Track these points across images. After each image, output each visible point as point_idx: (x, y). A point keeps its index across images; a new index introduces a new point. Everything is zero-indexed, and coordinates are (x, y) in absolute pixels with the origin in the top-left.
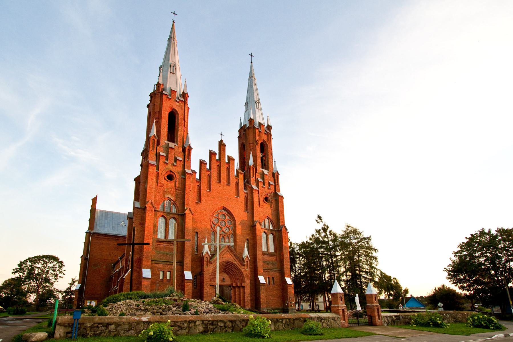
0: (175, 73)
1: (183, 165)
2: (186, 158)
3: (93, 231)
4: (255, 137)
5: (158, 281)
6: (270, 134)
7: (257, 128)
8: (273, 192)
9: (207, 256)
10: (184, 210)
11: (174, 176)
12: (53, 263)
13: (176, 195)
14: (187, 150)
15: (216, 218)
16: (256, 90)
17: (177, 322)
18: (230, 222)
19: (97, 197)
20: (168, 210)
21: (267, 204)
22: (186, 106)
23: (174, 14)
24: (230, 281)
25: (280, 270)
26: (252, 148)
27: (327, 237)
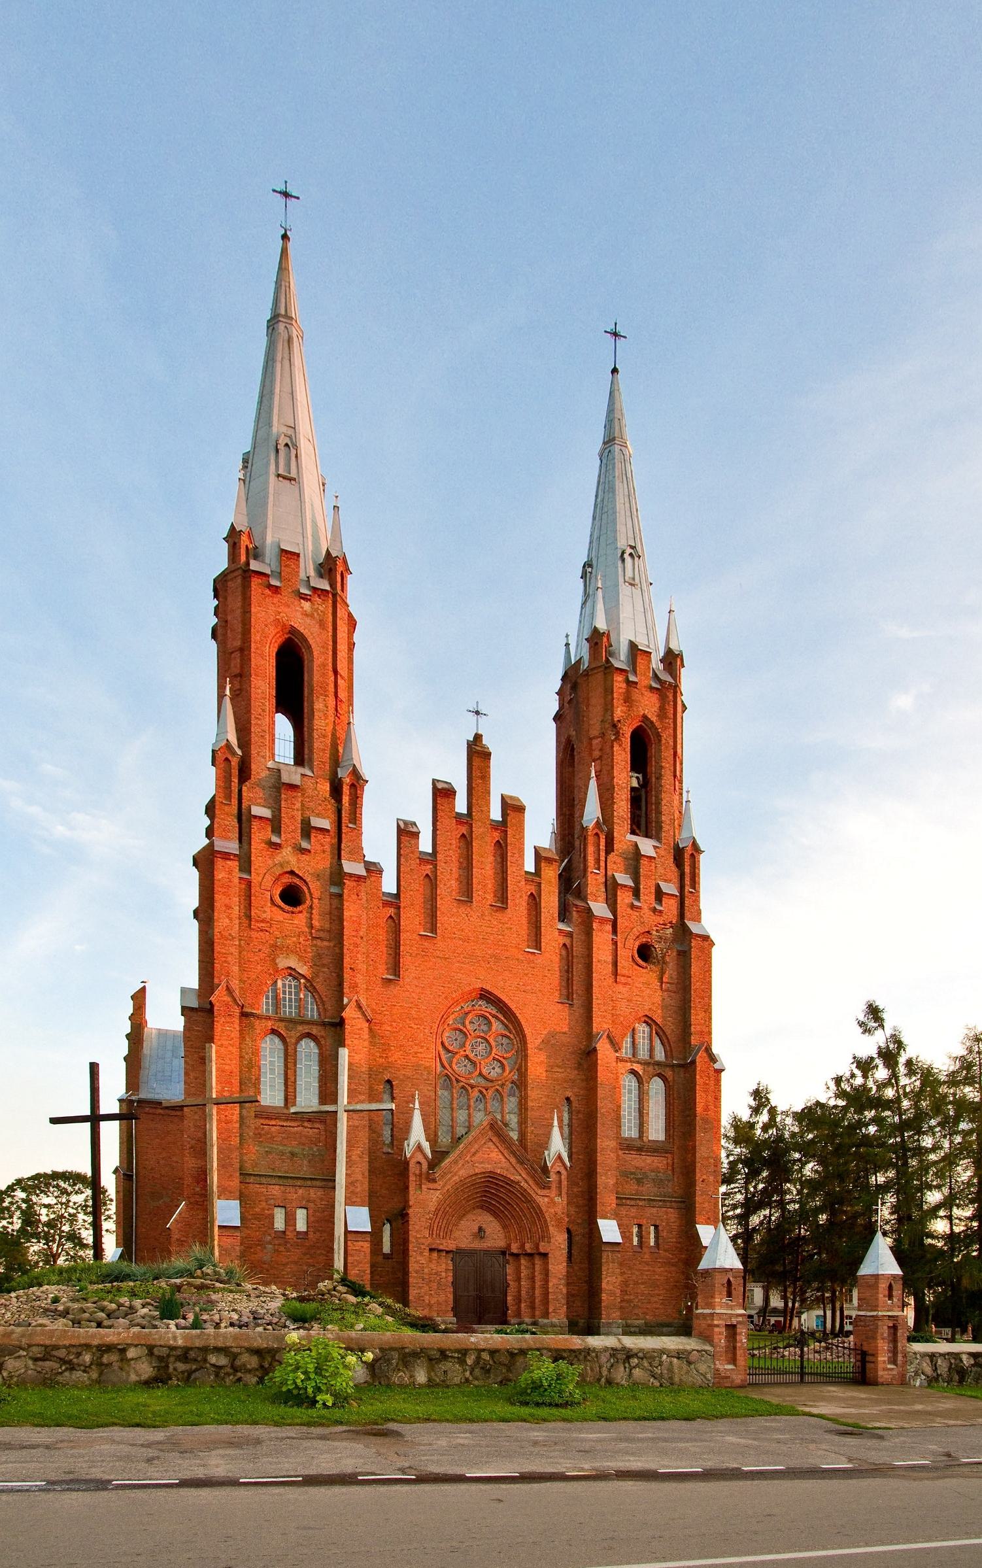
0: (293, 474)
1: (336, 846)
2: (345, 819)
3: (138, 1095)
4: (609, 707)
5: (269, 1235)
6: (675, 688)
7: (617, 669)
8: (671, 923)
9: (420, 1158)
10: (342, 1008)
11: (305, 888)
12: (82, 1192)
13: (313, 957)
14: (346, 789)
15: (456, 1029)
16: (627, 499)
17: (56, 1347)
18: (505, 1041)
19: (144, 988)
20: (289, 1011)
21: (644, 971)
22: (341, 613)
23: (286, 195)
24: (501, 1235)
25: (681, 1202)
26: (596, 754)
27: (897, 1083)
